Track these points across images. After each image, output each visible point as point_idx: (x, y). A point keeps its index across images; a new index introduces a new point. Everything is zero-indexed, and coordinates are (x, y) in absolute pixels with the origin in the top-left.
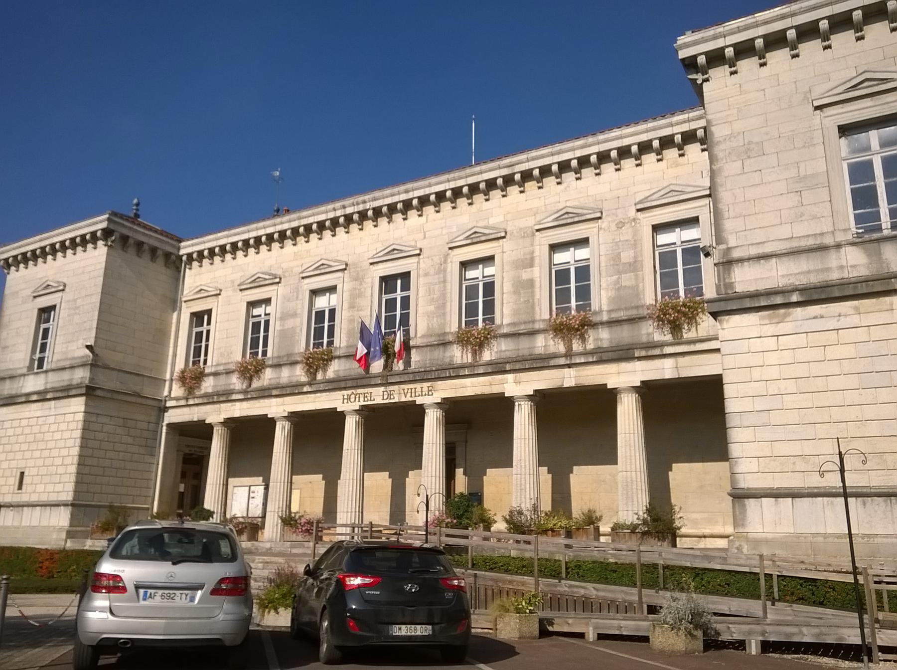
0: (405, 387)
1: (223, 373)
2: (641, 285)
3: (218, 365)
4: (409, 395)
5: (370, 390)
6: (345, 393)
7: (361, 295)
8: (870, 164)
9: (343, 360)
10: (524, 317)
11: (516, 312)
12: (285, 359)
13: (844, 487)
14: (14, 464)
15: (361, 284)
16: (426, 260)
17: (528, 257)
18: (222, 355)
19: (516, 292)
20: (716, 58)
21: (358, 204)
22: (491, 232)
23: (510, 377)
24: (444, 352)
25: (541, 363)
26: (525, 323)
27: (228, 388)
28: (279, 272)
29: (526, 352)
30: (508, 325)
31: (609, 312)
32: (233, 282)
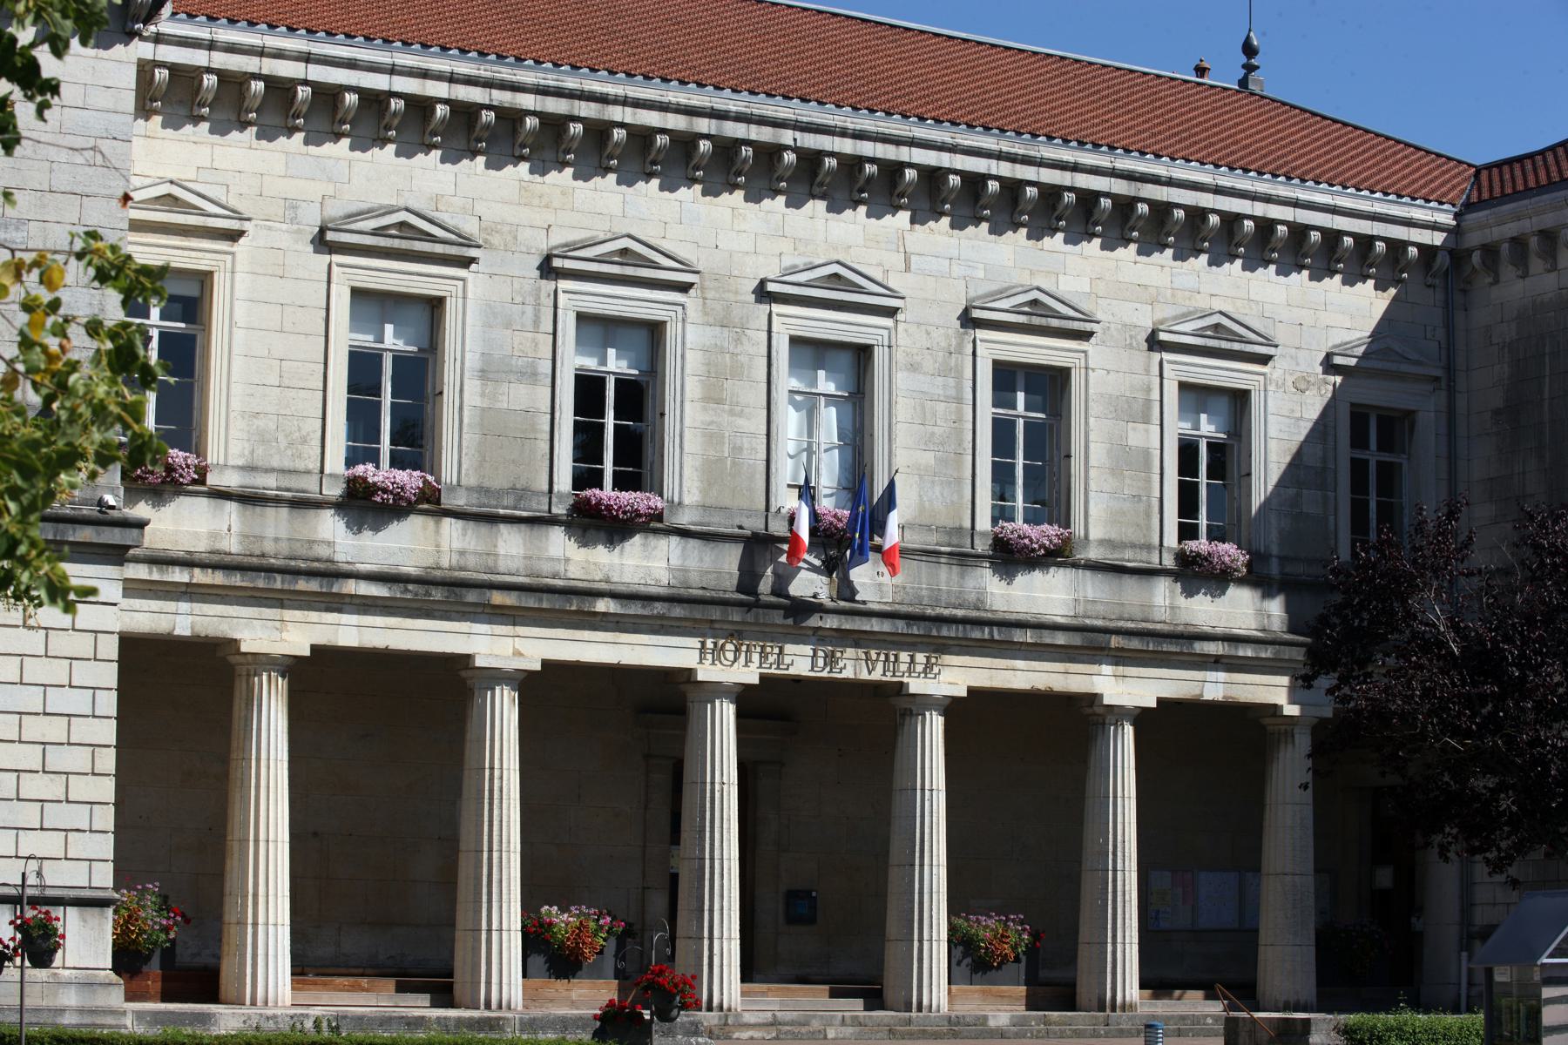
2: (1332, 518)
3: (250, 468)
4: (880, 666)
7: (737, 372)
10: (1131, 534)
11: (1114, 518)
15: (738, 341)
16: (913, 329)
17: (1140, 395)
18: (263, 438)
19: (1115, 471)
22: (1072, 313)
24: (962, 576)
25: (321, 585)
26: (1133, 546)
28: (470, 227)
30: (1102, 542)
31: (1283, 559)
32: (292, 205)
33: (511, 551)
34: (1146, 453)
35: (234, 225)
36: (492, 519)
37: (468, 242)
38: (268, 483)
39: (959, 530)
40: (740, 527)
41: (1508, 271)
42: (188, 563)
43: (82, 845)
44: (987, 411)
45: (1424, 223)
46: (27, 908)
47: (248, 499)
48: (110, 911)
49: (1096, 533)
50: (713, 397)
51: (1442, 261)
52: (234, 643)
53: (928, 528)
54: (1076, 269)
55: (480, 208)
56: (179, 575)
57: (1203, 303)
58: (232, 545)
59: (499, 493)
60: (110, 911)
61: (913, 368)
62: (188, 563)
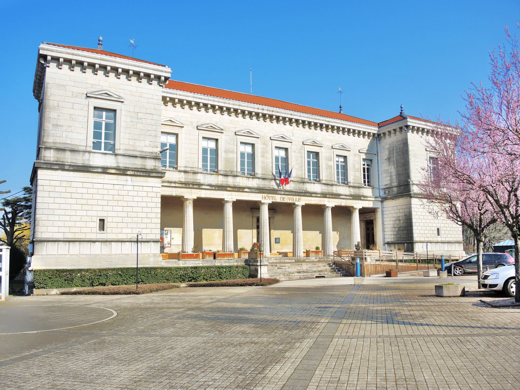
0: (290, 197)
1: (191, 173)
5: (275, 195)
6: (263, 195)
8: (101, 123)
9: (260, 180)
10: (330, 179)
12: (230, 173)
13: (137, 239)
14: (434, 225)
19: (327, 169)
20: (56, 59)
21: (270, 111)
23: (326, 199)
27: (195, 181)
28: (222, 127)
29: (331, 191)
32: (192, 122)
33: (230, 181)
34: (331, 166)
35: (182, 125)
36: (227, 176)
37: (222, 130)
38: (188, 169)
39: (303, 178)
40: (210, 250)
41: (387, 136)
42: (175, 183)
43: (154, 231)
44: (306, 159)
45: (374, 130)
46: (301, 233)
47: (185, 172)
48: (159, 243)
49: (324, 179)
50: (263, 156)
51: (376, 135)
52: (183, 197)
53: (298, 178)
54: (320, 135)
55: (224, 124)
56: (173, 185)
57: (339, 142)
58: (183, 180)
59: (228, 171)
60: (159, 243)
61: (295, 152)
62: (175, 183)
